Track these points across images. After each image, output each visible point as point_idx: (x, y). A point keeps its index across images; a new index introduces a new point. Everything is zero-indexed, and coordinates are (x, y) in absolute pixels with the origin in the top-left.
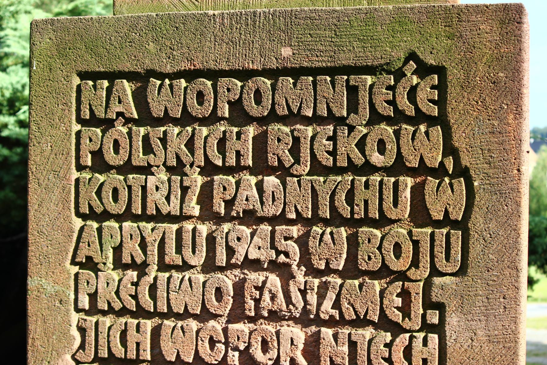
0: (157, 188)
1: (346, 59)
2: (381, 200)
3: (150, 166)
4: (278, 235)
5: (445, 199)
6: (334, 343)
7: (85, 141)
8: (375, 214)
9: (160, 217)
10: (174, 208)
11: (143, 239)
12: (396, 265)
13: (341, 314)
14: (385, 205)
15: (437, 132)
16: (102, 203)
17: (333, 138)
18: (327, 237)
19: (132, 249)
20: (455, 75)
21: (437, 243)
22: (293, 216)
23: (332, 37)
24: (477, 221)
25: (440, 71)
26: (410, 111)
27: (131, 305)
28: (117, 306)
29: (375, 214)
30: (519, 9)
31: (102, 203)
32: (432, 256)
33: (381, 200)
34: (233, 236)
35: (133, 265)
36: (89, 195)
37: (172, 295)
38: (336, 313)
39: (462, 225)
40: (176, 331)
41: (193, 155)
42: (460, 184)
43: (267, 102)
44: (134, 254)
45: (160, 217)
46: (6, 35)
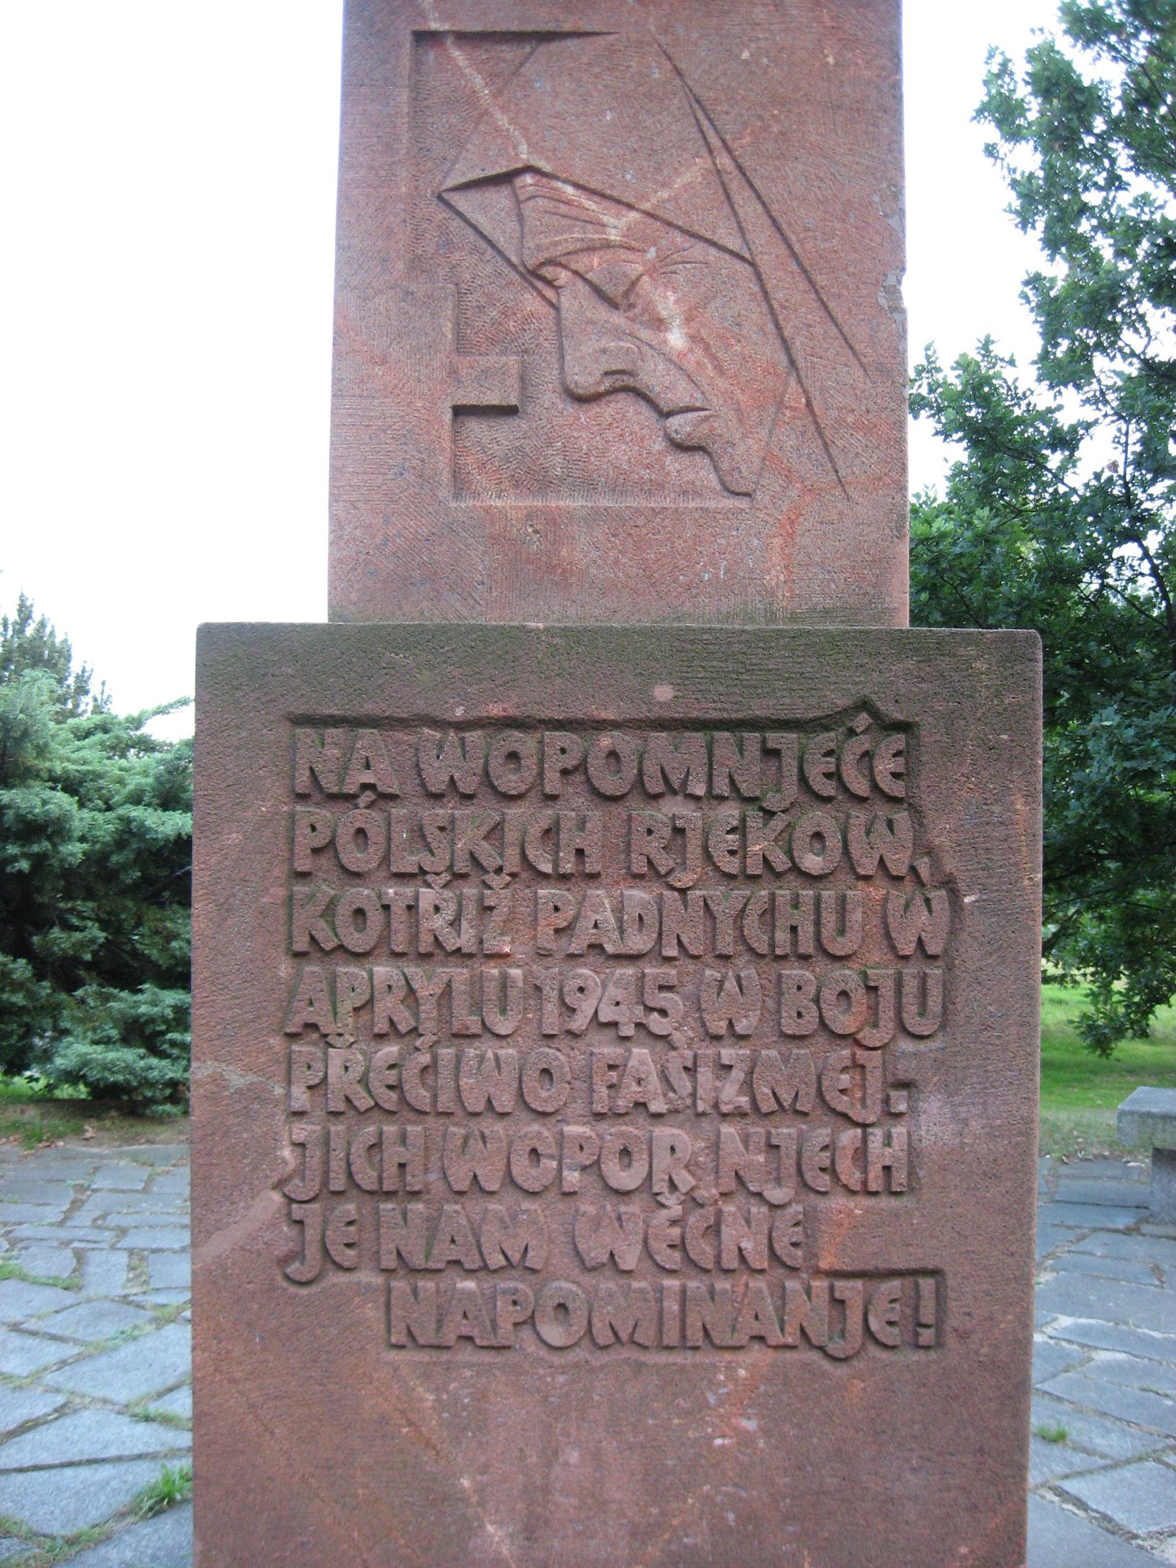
0: (437, 909)
1: (759, 709)
2: (818, 924)
3: (423, 872)
4: (649, 984)
5: (923, 923)
6: (742, 1148)
7: (302, 830)
8: (807, 945)
9: (436, 953)
10: (466, 939)
11: (411, 991)
12: (843, 1022)
13: (754, 1101)
14: (825, 933)
15: (902, 817)
16: (336, 935)
17: (740, 829)
18: (731, 985)
19: (388, 1006)
20: (931, 735)
21: (906, 990)
22: (672, 952)
23: (738, 673)
24: (970, 953)
25: (903, 727)
26: (860, 786)
27: (390, 1100)
28: (364, 1102)
29: (807, 945)
30: (212, 639)
31: (336, 935)
32: (899, 1009)
33: (818, 924)
34: (571, 985)
35: (393, 1032)
36: (307, 919)
37: (465, 1082)
38: (744, 1100)
39: (945, 959)
40: (471, 1142)
41: (501, 855)
42: (939, 896)
43: (630, 772)
44: (395, 1019)
45: (436, 953)
46: (42, 625)
